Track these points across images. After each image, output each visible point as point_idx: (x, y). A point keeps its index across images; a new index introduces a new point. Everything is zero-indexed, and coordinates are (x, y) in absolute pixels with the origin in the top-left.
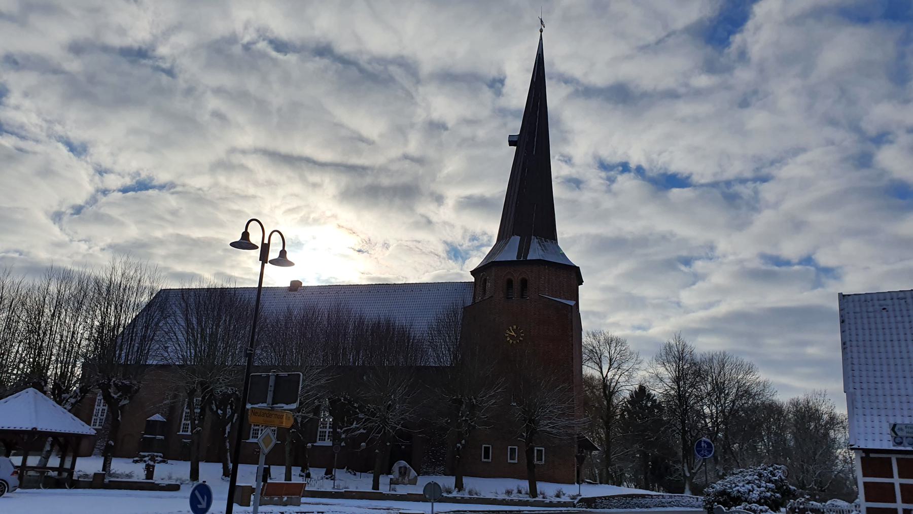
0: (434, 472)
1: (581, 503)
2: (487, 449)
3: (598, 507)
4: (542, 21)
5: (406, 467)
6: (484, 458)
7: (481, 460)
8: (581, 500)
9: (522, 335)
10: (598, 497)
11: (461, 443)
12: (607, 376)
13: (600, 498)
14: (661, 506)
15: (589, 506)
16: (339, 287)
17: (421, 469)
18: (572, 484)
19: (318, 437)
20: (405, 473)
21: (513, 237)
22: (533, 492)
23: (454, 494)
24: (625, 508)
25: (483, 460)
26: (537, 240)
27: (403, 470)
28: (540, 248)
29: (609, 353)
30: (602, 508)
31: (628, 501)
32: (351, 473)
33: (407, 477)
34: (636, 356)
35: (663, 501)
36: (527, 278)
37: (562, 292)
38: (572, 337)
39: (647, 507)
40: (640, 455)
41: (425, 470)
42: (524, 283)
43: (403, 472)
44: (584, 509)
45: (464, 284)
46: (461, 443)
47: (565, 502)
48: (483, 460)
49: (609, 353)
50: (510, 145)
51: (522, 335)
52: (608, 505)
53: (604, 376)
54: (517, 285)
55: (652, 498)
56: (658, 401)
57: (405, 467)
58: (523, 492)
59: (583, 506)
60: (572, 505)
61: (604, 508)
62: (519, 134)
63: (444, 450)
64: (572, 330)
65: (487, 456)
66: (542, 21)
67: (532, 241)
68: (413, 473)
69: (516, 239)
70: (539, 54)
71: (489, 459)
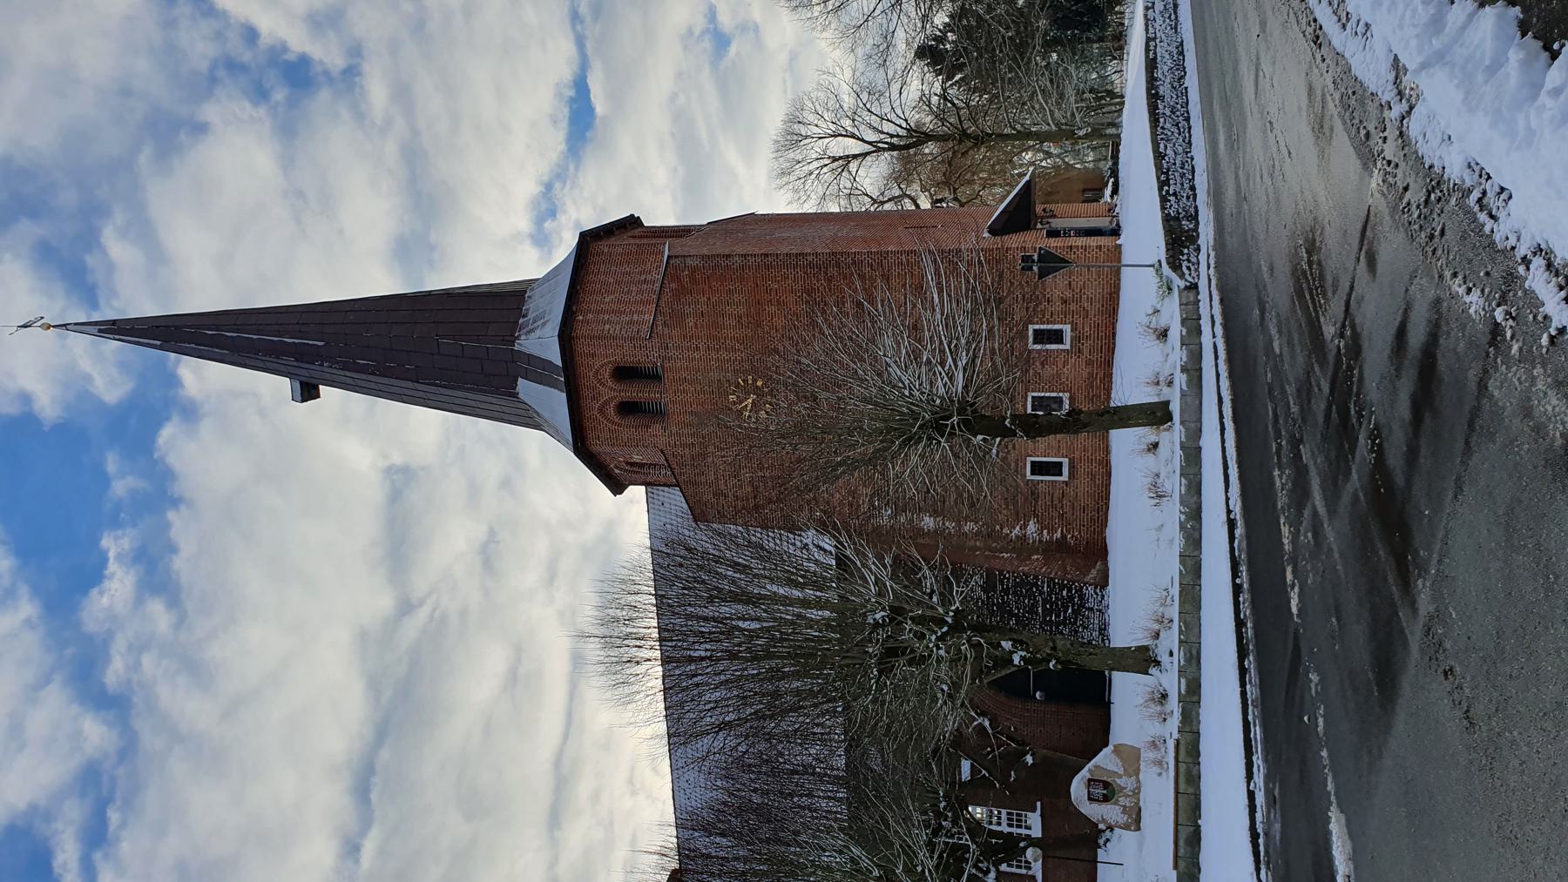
0: (1100, 611)
1: (1185, 264)
2: (1038, 468)
3: (1192, 210)
4: (25, 326)
5: (1090, 780)
6: (1061, 475)
7: (1066, 483)
8: (1175, 266)
9: (750, 382)
10: (1163, 208)
11: (1011, 653)
12: (869, 143)
13: (1164, 200)
14: (1176, 13)
15: (1192, 238)
16: (676, 792)
17: (1094, 642)
18: (1120, 253)
19: (1024, 871)
20: (1106, 785)
21: (521, 396)
22: (1156, 415)
23: (1169, 679)
24: (1188, 119)
25: (1065, 477)
26: (523, 337)
27: (1099, 791)
28: (538, 333)
29: (820, 138)
30: (1195, 196)
31: (1168, 112)
32: (1108, 840)
33: (1118, 781)
34: (825, 76)
35: (1162, 8)
36: (609, 368)
37: (643, 277)
38: (745, 256)
39: (1181, 53)
40: (1055, 51)
41: (1095, 634)
42: (625, 373)
43: (1105, 790)
44: (1203, 257)
45: (650, 505)
46: (1011, 653)
47: (1183, 322)
48: (1065, 477)
49: (820, 138)
50: (318, 396)
51: (750, 382)
52: (1183, 175)
53: (869, 148)
54: (633, 392)
55: (1155, 39)
56: (947, 20)
57: (1091, 782)
58: (1153, 438)
59: (1194, 260)
60: (1192, 296)
61: (1193, 188)
62: (288, 379)
63: (1043, 582)
64: (728, 256)
65: (1056, 469)
66: (25, 326)
67: (523, 349)
68: (1105, 759)
69: (525, 387)
70: (100, 331)
71: (1061, 463)
